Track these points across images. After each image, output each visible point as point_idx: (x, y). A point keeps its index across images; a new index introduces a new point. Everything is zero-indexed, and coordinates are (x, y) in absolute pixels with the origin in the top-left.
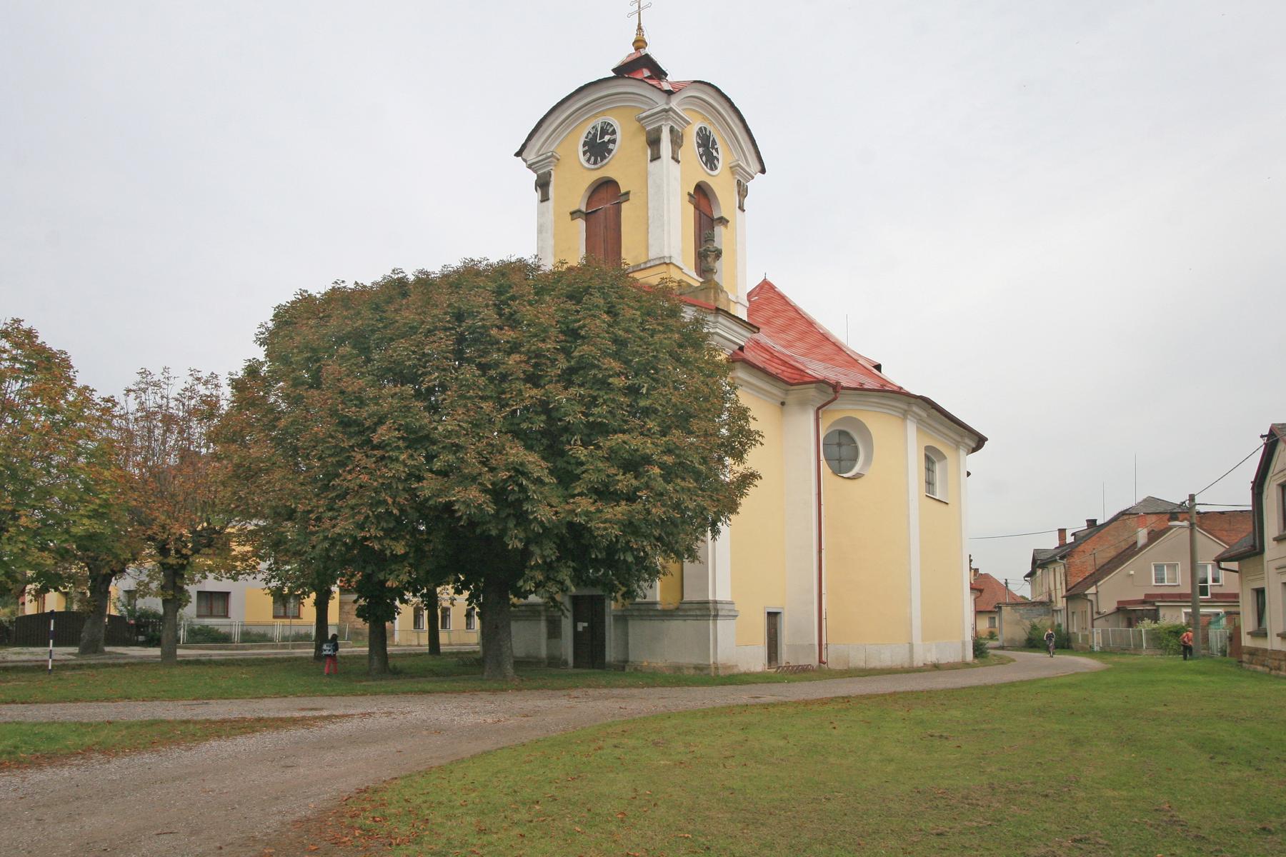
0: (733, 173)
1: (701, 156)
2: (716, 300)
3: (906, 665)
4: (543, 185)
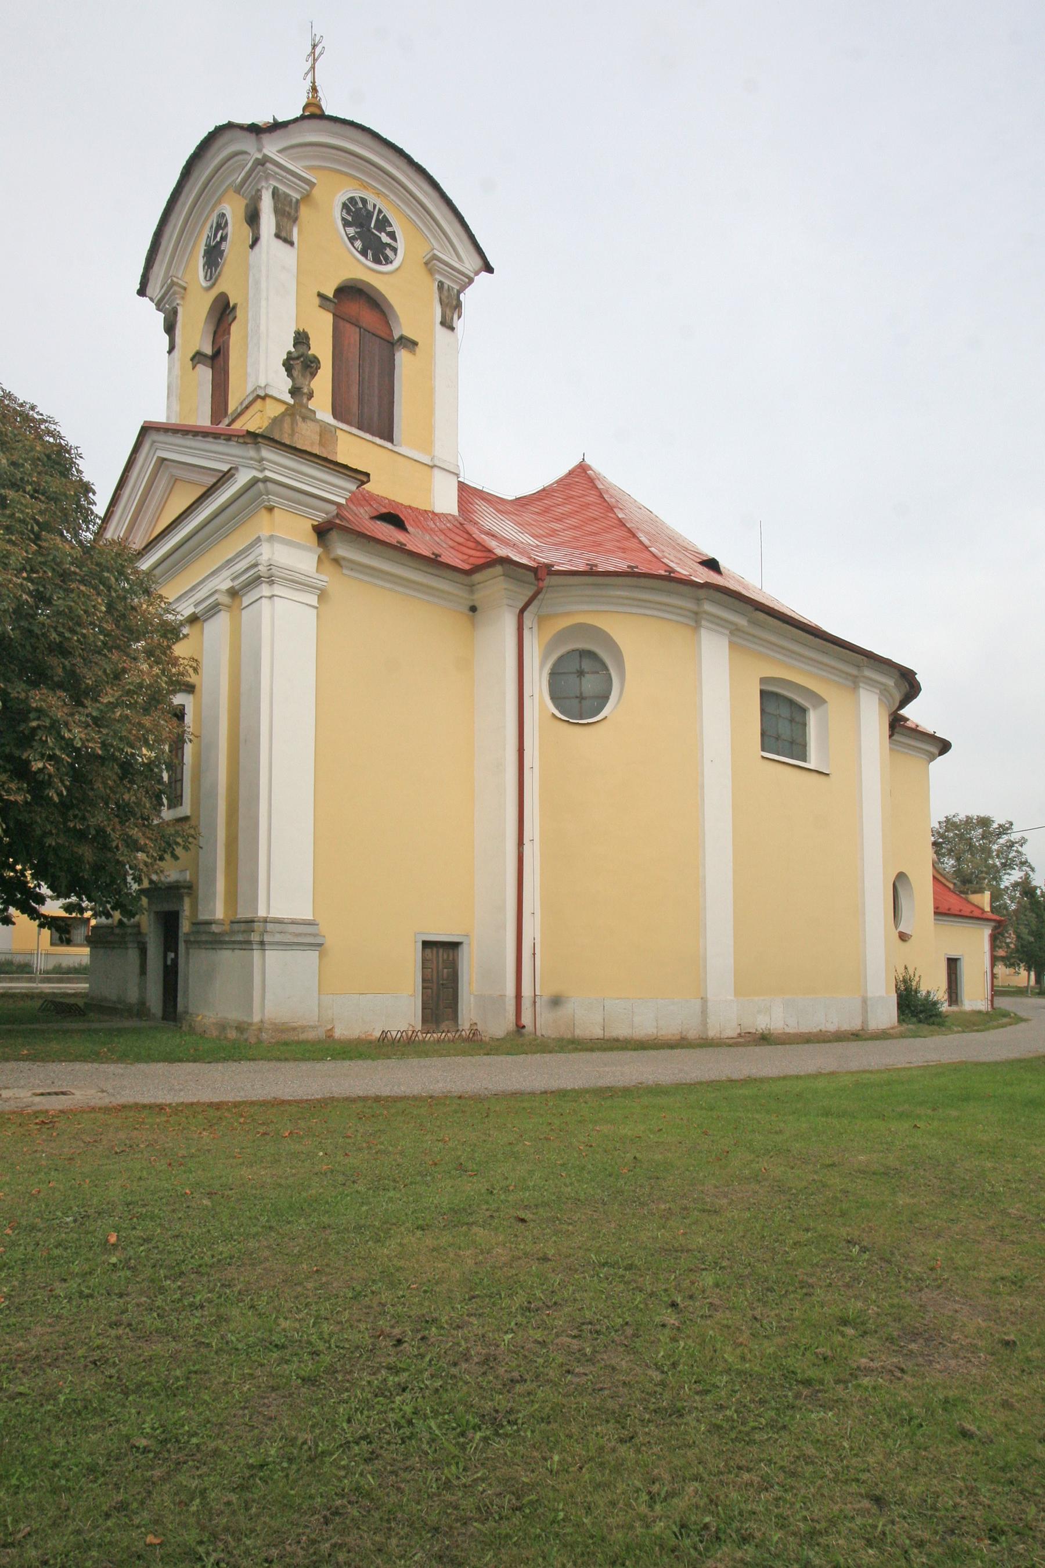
0: (431, 272)
1: (352, 240)
2: (293, 433)
3: (692, 1034)
4: (170, 328)
